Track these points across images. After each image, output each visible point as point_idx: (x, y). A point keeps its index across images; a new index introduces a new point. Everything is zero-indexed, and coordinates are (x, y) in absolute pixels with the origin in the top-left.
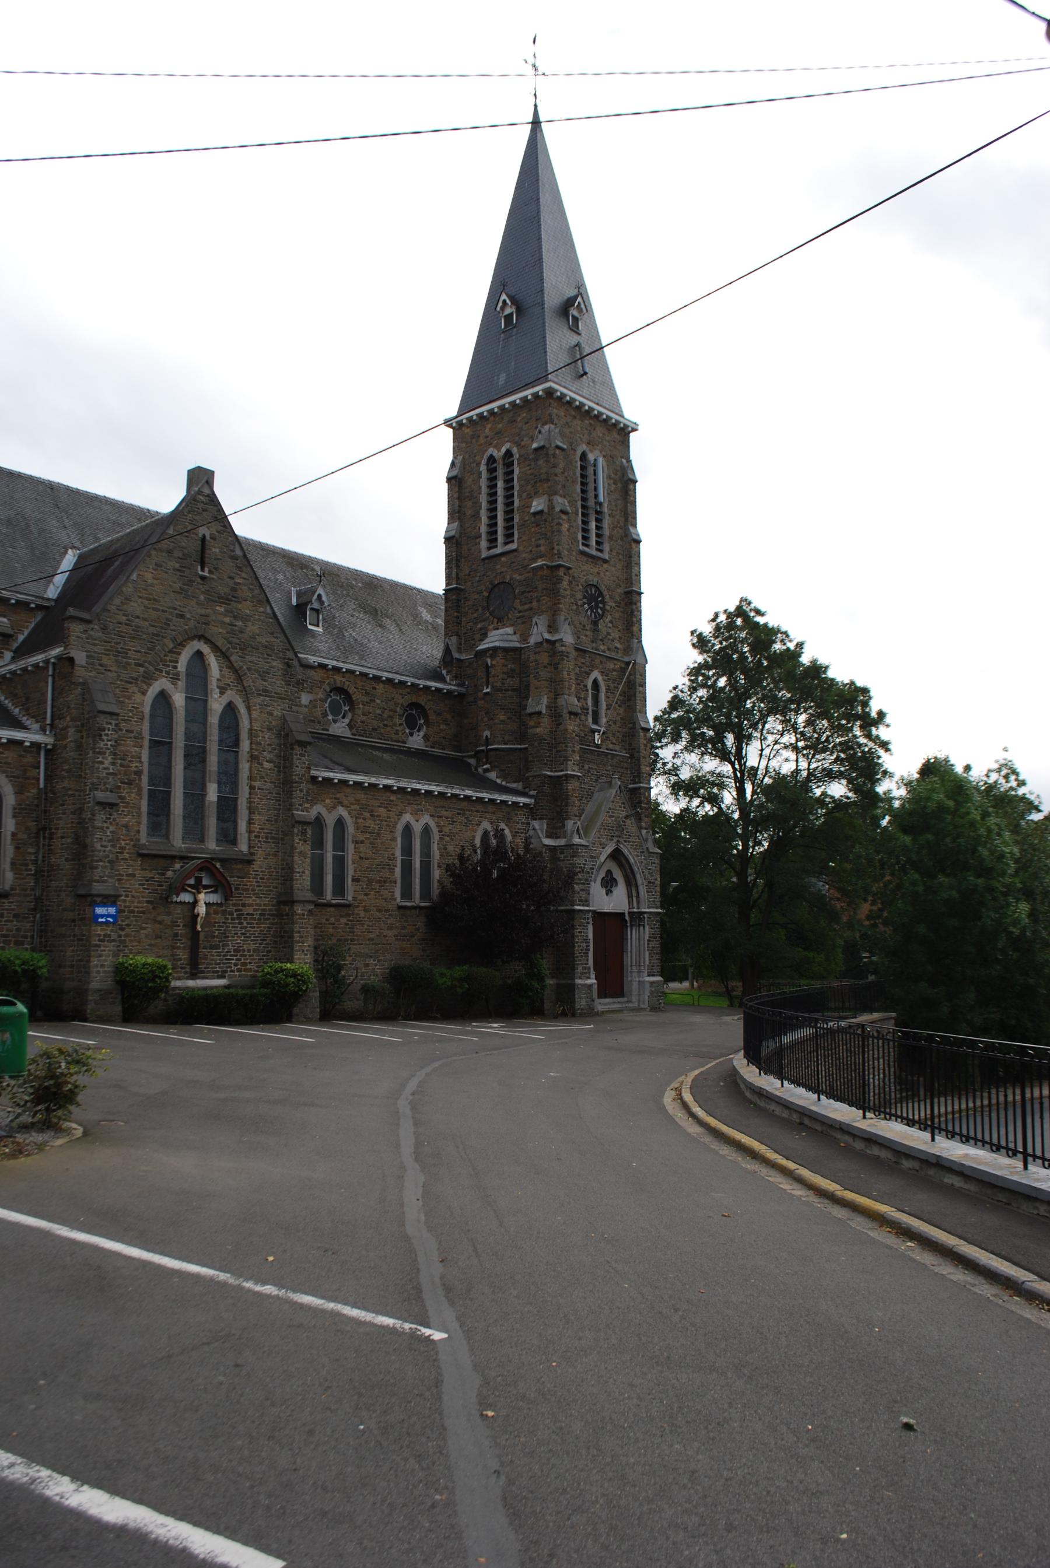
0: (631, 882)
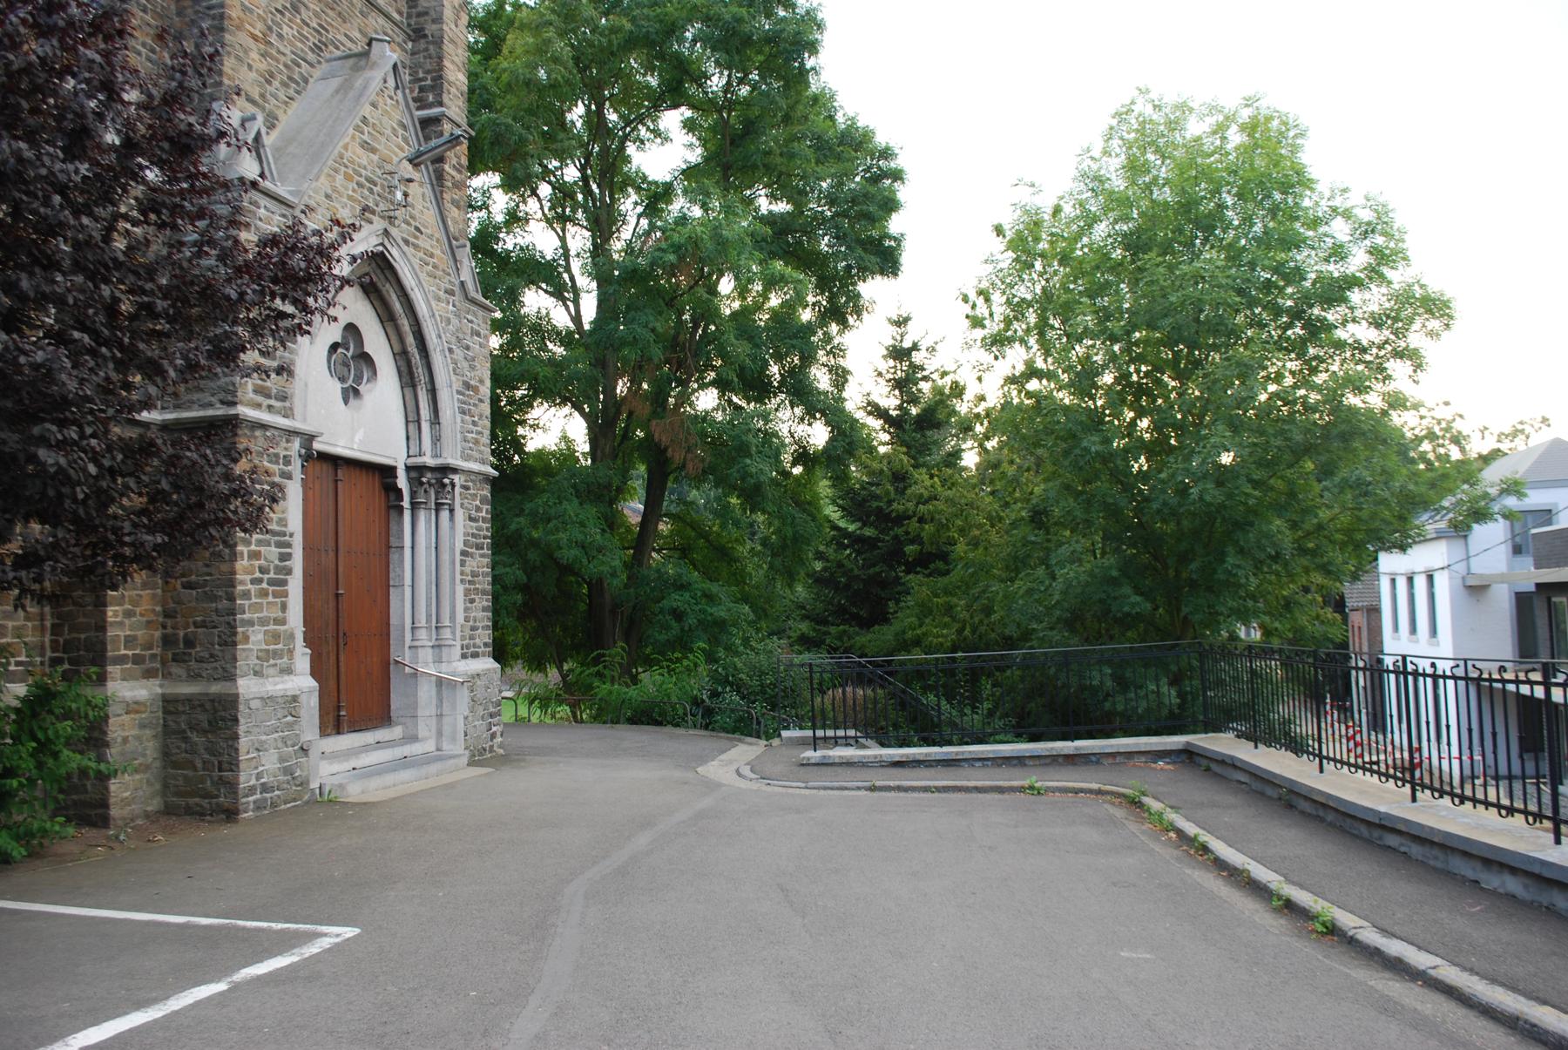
0: (414, 370)
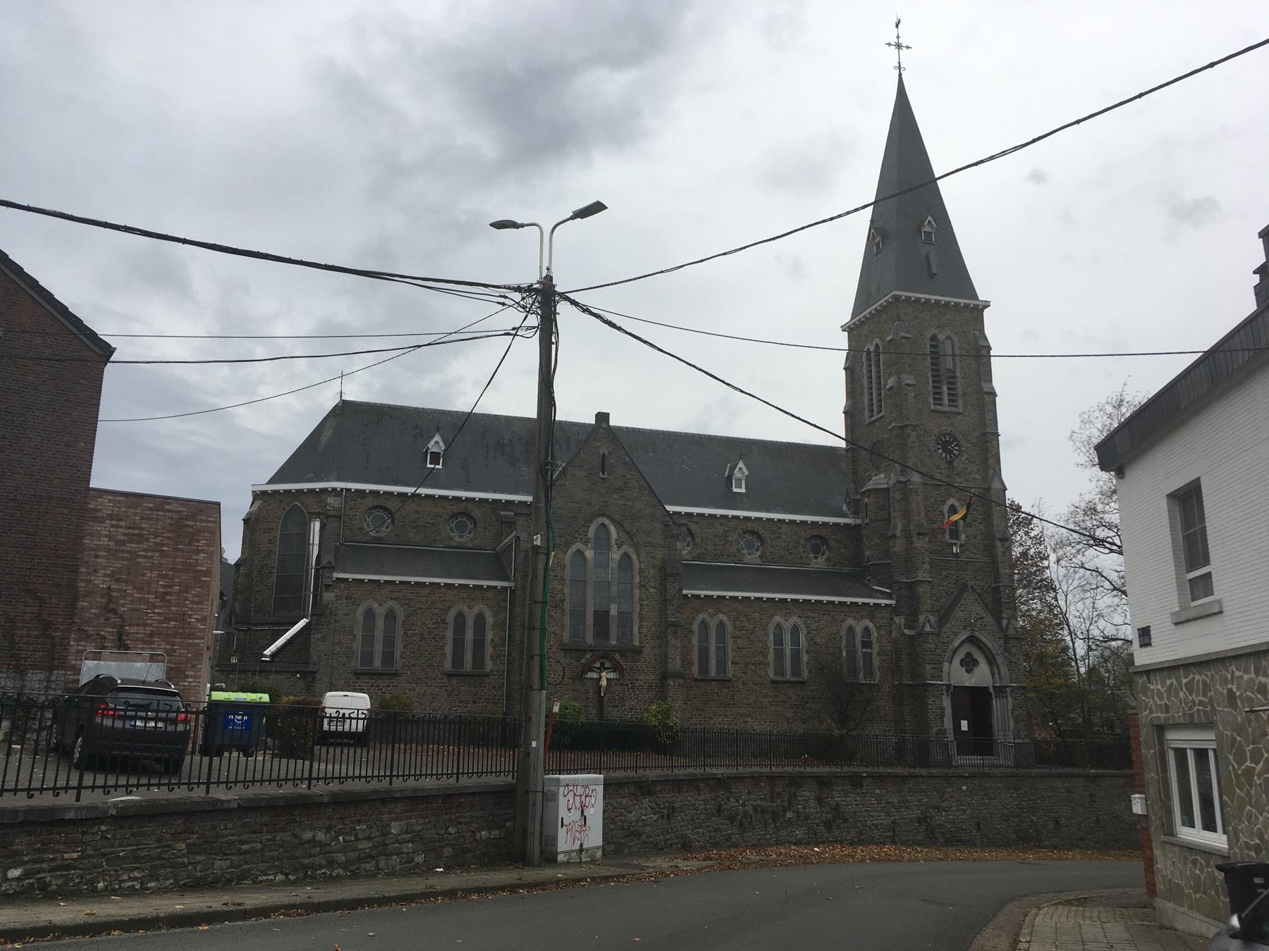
0: (991, 661)
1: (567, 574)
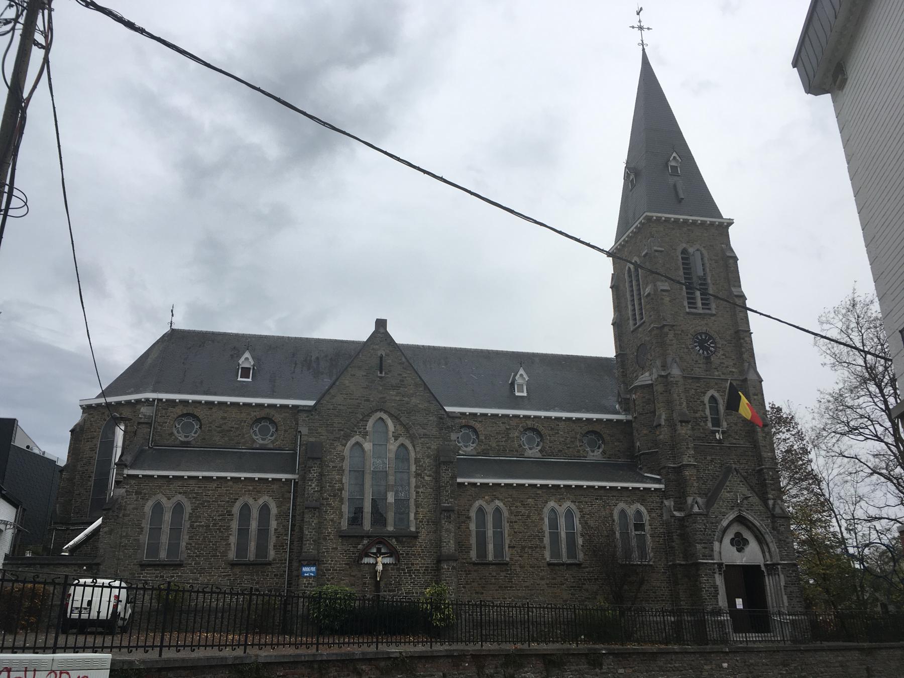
0: (761, 540)
1: (346, 465)
